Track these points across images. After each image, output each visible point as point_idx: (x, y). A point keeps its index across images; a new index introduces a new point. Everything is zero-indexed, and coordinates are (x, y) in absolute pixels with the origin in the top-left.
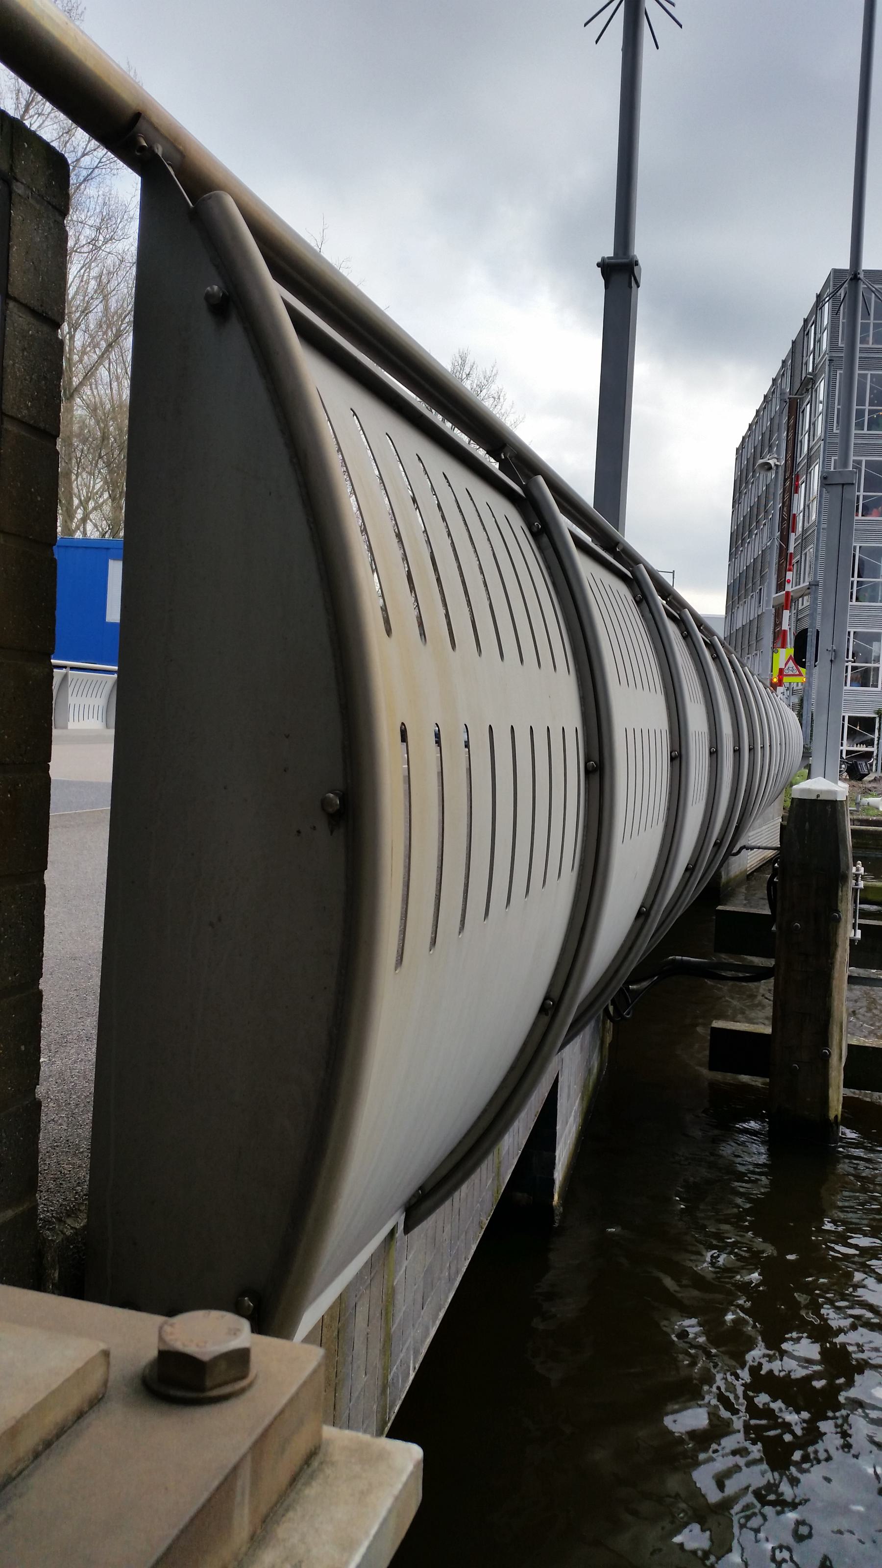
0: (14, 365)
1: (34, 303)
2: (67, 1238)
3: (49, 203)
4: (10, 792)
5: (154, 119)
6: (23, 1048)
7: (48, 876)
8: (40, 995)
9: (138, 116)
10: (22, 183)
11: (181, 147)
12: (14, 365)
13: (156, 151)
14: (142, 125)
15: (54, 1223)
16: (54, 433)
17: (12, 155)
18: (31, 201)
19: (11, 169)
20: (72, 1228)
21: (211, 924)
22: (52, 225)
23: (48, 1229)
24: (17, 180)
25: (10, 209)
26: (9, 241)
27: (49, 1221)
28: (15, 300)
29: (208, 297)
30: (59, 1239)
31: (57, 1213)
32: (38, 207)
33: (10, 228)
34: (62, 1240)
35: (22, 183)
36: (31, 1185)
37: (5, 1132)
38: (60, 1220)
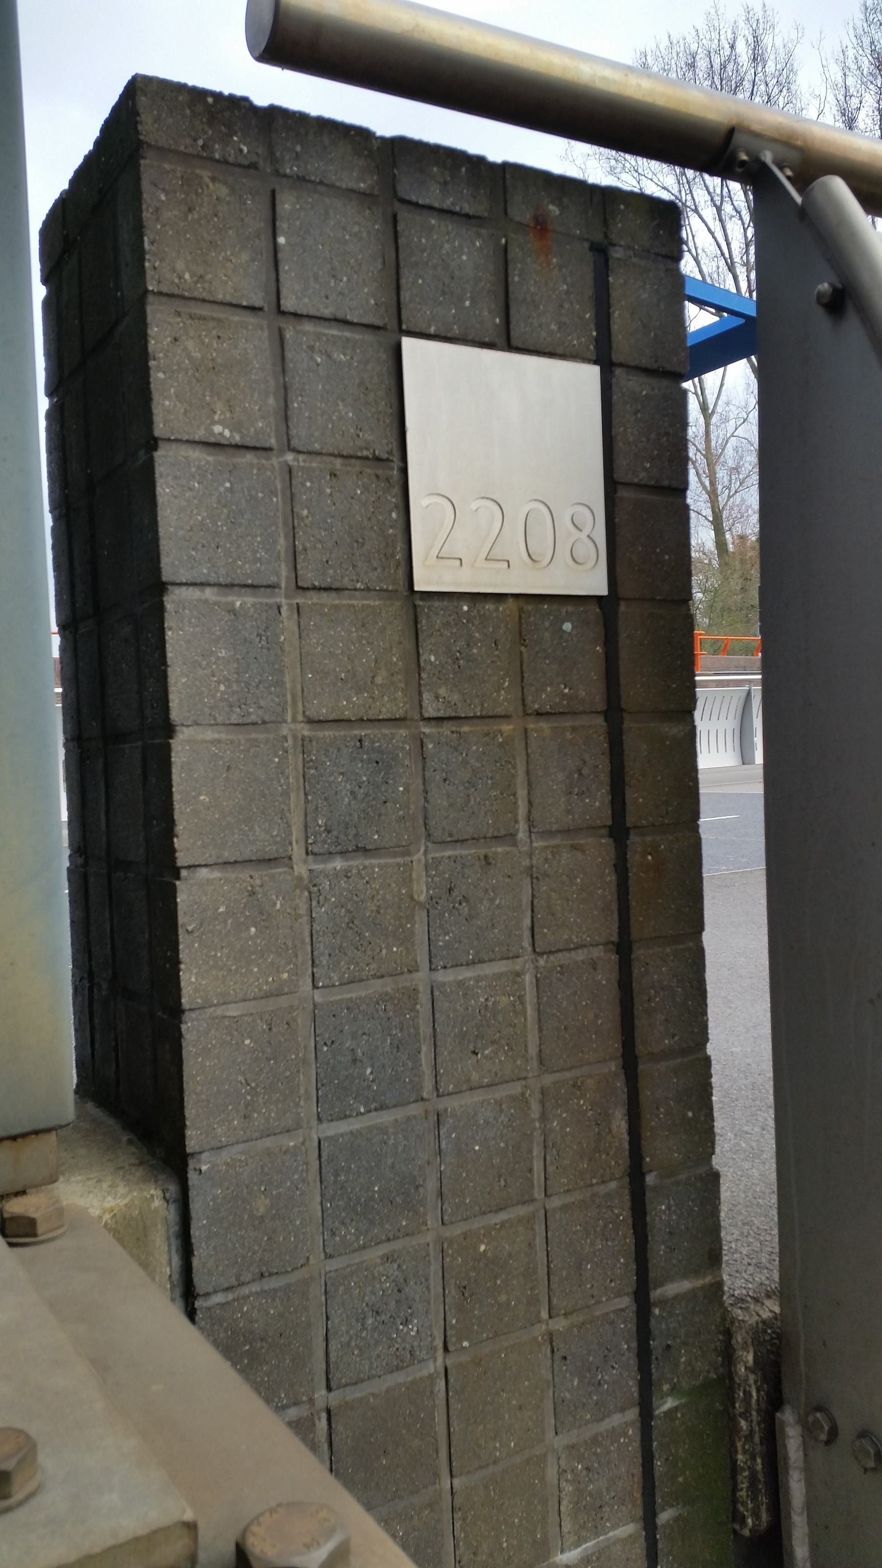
0: (625, 430)
1: (645, 362)
2: (764, 1322)
3: (657, 254)
4: (650, 854)
5: (756, 127)
6: (690, 1114)
7: (706, 937)
8: (707, 1061)
9: (731, 132)
10: (620, 246)
11: (799, 143)
12: (625, 430)
13: (763, 158)
14: (739, 139)
15: (748, 1302)
16: (674, 484)
17: (605, 223)
18: (634, 260)
19: (606, 236)
20: (771, 1311)
21: (872, 1001)
22: (663, 275)
23: (741, 1308)
24: (615, 245)
25: (608, 276)
26: (609, 308)
27: (742, 1300)
28: (621, 365)
29: (820, 296)
30: (752, 1320)
31: (754, 1292)
32: (643, 263)
33: (609, 296)
34: (757, 1323)
35: (620, 246)
36: (714, 1257)
37: (674, 1199)
38: (756, 1300)
